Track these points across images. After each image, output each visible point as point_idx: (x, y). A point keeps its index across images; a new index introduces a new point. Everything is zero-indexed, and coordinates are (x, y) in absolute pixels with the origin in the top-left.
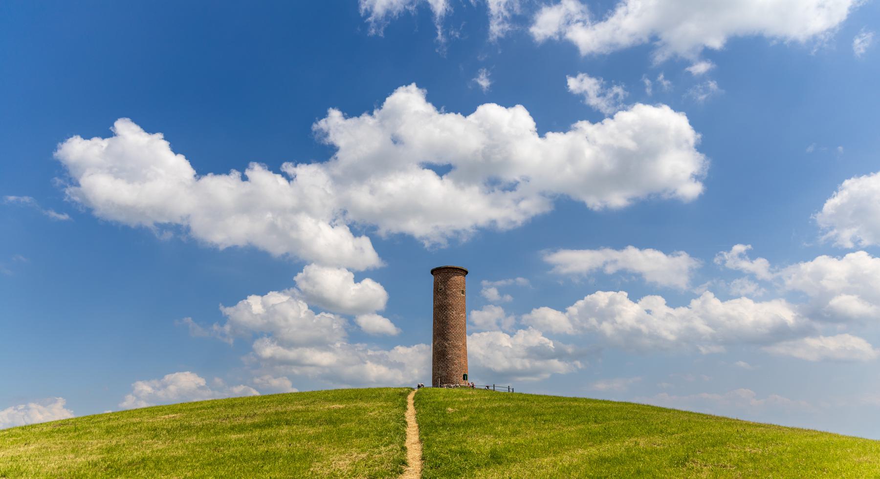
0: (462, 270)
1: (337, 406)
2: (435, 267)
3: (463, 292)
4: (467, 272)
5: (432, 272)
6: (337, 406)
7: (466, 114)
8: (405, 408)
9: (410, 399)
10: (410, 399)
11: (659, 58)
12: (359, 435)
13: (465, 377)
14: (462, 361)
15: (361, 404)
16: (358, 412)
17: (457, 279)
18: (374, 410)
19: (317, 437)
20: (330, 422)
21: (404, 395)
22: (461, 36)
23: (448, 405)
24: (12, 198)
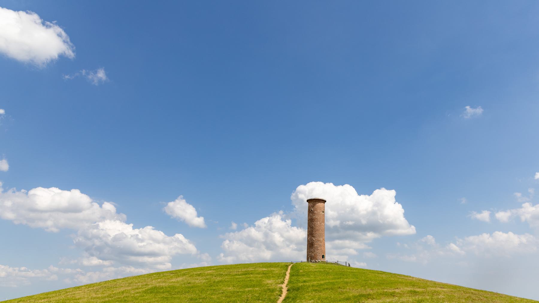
1: (264, 269)
3: (323, 212)
4: (324, 201)
5: (308, 201)
6: (264, 269)
7: (369, 195)
8: (287, 270)
9: (290, 267)
10: (290, 267)
11: (313, 238)
12: (273, 277)
15: (272, 269)
16: (271, 271)
17: (320, 205)
18: (276, 270)
19: (262, 277)
20: (264, 274)
21: (287, 266)
23: (301, 269)
24: (67, 77)
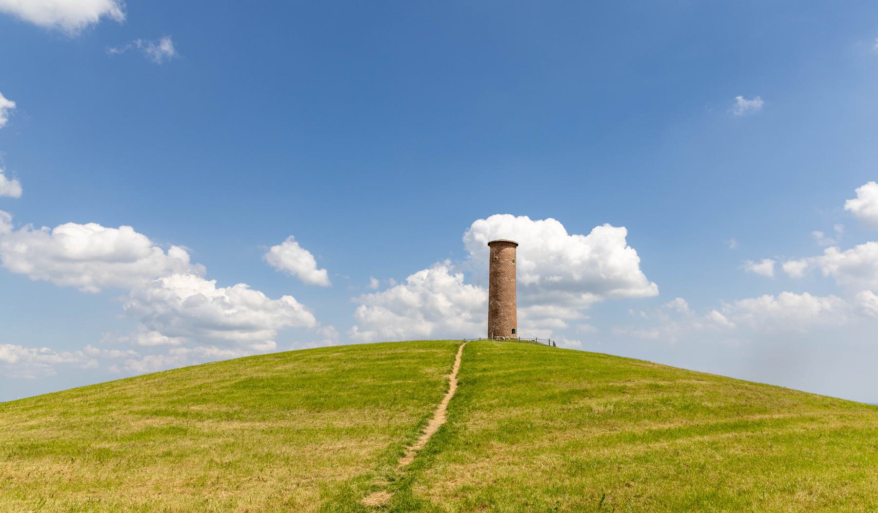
0: (494, 261)
1: (421, 351)
2: (492, 240)
3: (513, 261)
4: (515, 245)
5: (489, 244)
6: (421, 351)
8: (457, 353)
9: (461, 348)
10: (461, 348)
12: (435, 363)
13: (514, 331)
14: (513, 318)
15: (434, 350)
16: (433, 354)
17: (508, 250)
18: (441, 353)
19: (418, 363)
22: (431, 279)
23: (479, 351)
